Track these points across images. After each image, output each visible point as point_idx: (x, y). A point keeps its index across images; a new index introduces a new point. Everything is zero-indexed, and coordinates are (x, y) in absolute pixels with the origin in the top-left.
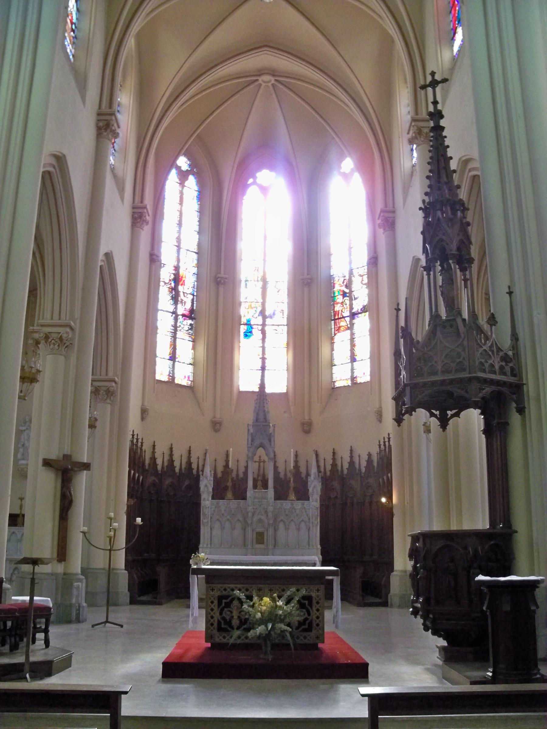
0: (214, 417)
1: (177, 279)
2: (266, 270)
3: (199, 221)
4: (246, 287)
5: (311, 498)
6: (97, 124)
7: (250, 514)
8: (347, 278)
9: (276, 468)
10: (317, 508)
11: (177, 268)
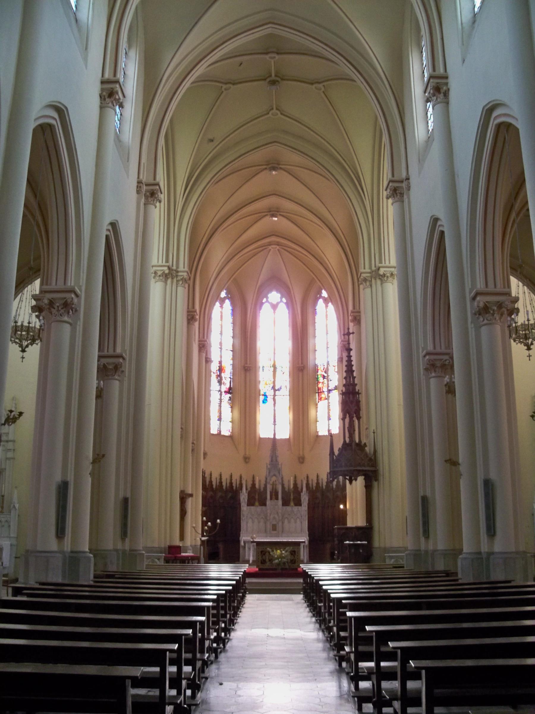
0: (245, 454)
1: (221, 369)
2: (275, 360)
3: (233, 330)
4: (263, 371)
5: (302, 505)
6: (187, 317)
7: (269, 514)
8: (326, 367)
9: (283, 485)
10: (306, 511)
11: (220, 362)
